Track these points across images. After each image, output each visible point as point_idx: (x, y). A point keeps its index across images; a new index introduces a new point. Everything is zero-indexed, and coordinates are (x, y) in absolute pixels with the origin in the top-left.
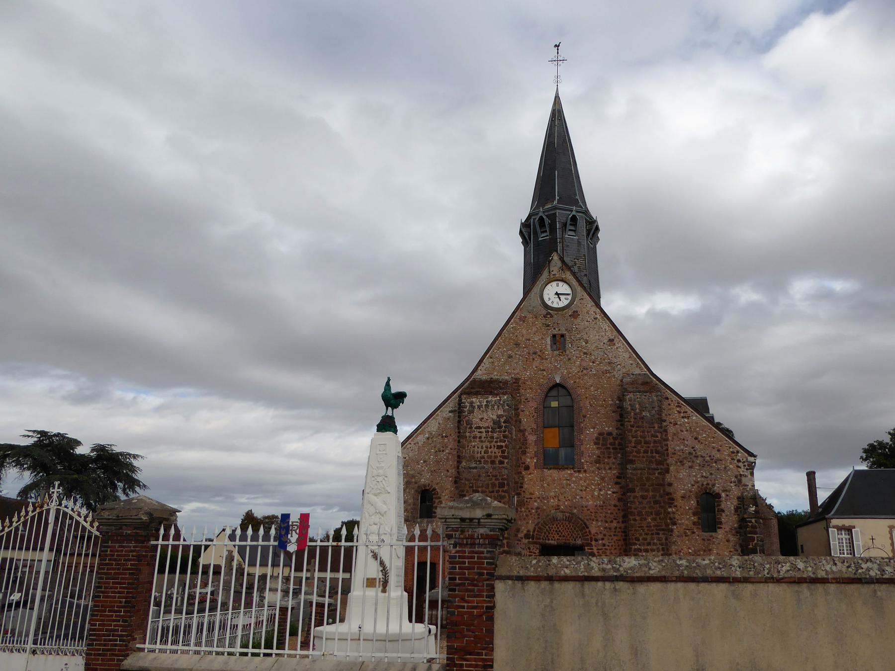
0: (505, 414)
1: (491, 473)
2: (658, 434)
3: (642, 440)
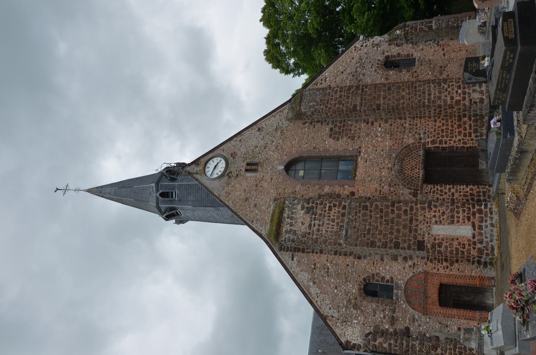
0: (301, 203)
1: (353, 217)
2: (335, 90)
3: (338, 100)
